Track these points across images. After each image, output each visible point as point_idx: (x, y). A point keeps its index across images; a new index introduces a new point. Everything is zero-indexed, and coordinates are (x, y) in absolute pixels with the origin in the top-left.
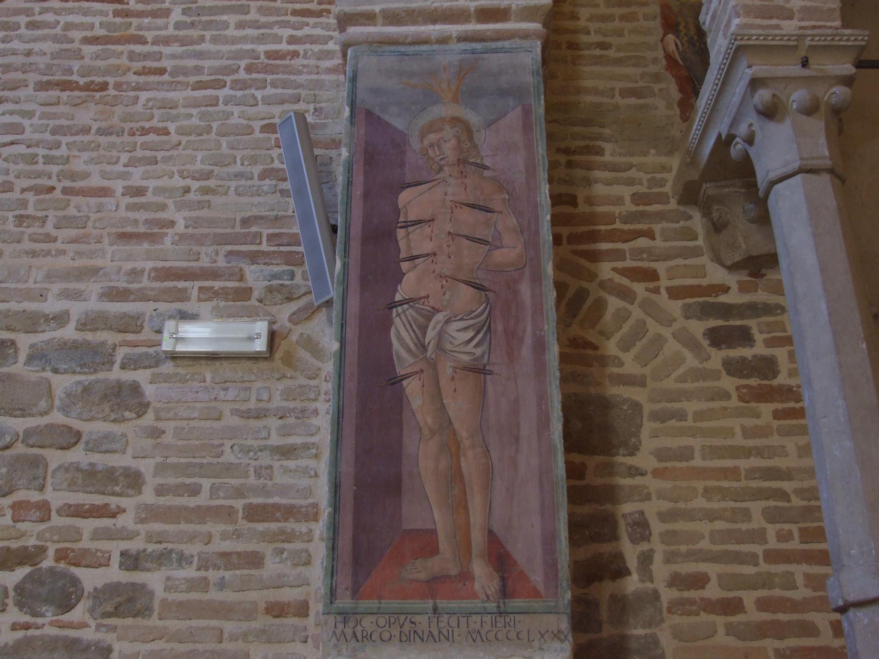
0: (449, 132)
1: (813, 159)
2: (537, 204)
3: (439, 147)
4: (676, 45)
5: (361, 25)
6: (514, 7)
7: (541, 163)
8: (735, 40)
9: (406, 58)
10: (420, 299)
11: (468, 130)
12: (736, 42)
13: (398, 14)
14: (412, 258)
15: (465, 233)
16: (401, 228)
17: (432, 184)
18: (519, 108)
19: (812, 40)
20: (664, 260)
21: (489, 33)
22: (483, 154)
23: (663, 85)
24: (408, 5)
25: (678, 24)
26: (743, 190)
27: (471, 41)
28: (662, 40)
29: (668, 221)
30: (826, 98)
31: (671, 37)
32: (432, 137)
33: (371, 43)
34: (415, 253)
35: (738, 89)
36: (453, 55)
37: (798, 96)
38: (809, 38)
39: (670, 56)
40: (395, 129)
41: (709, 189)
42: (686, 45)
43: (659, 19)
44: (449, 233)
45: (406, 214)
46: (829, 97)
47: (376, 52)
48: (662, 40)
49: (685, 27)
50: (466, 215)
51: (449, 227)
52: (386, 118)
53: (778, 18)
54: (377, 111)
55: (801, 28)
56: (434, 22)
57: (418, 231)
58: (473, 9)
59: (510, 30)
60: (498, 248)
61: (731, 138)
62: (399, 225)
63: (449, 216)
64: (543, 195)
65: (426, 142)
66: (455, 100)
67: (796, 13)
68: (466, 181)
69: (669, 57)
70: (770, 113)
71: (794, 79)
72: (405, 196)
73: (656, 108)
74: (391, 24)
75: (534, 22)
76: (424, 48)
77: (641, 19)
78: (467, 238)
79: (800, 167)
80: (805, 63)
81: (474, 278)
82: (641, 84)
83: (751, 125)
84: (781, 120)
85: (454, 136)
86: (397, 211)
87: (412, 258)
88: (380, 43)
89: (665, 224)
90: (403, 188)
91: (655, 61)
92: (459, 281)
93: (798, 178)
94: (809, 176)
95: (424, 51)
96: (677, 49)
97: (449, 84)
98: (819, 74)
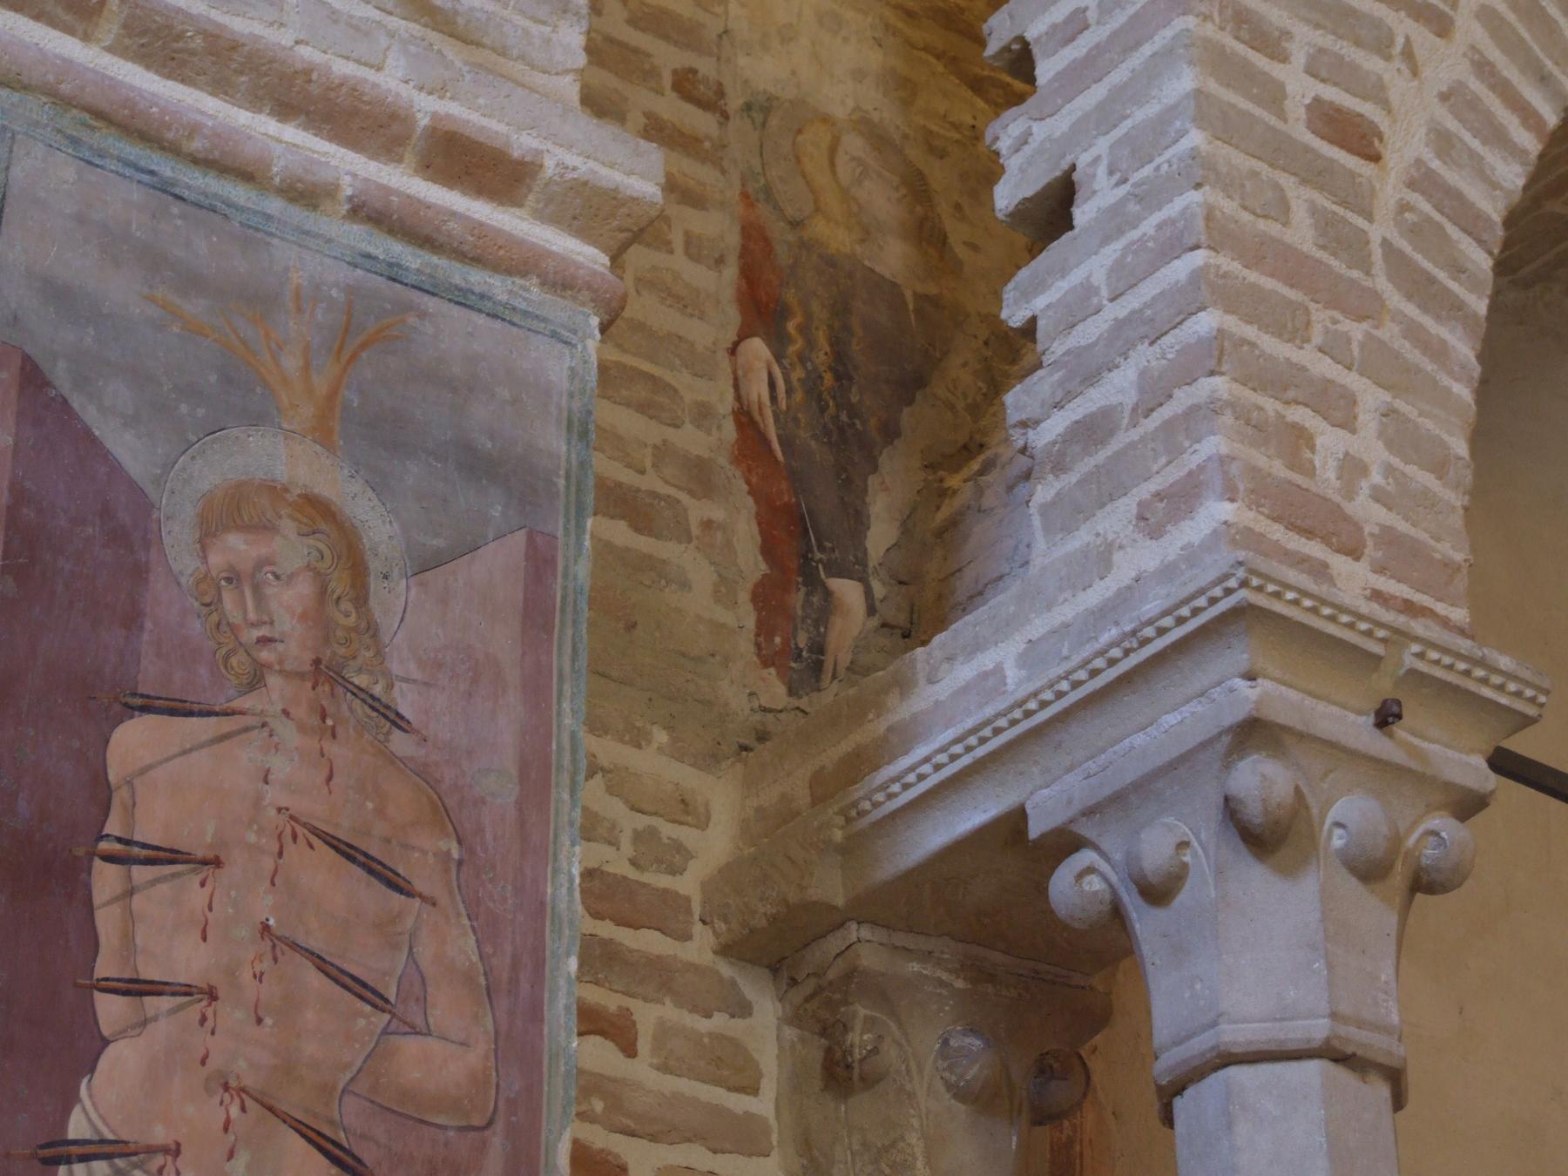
0: (291, 548)
1: (1361, 1024)
2: (543, 904)
3: (257, 590)
4: (772, 385)
5: (37, 17)
6: (549, 164)
7: (566, 761)
8: (1244, 584)
9: (176, 208)
10: (151, 1150)
11: (351, 557)
12: (1244, 593)
13: (180, 37)
14: (137, 988)
15: (315, 944)
16: (109, 858)
17: (227, 724)
18: (520, 537)
19: (1420, 656)
20: (654, 1138)
22: (395, 668)
23: (718, 514)
24: (215, 15)
25: (784, 313)
26: (960, 984)
27: (391, 232)
28: (733, 351)
29: (679, 1004)
30: (1411, 842)
31: (757, 347)
32: (237, 547)
33: (64, 102)
34: (149, 972)
35: (1171, 719)
36: (321, 258)
37: (1349, 814)
38: (1416, 648)
39: (748, 414)
40: (116, 469)
41: (868, 948)
42: (799, 396)
43: (731, 272)
44: (266, 928)
45: (130, 810)
46: (1418, 841)
47: (75, 142)
48: (733, 351)
50: (317, 871)
51: (264, 906)
52: (90, 414)
53: (1326, 540)
54: (60, 375)
55: (1377, 596)
56: (285, 110)
57: (164, 888)
58: (424, 121)
59: (521, 243)
60: (416, 1032)
61: (1065, 843)
62: (104, 846)
63: (268, 863)
64: (563, 878)
65: (216, 559)
66: (322, 433)
67: (1370, 543)
68: (333, 749)
69: (745, 418)
70: (1265, 838)
71: (1353, 754)
72: (133, 742)
73: (685, 585)
74: (144, 57)
75: (594, 242)
76: (238, 193)
78: (321, 964)
79: (1328, 1040)
80: (1386, 718)
81: (332, 1122)
82: (650, 482)
83: (1183, 845)
84: (1289, 871)
85: (308, 567)
86: (101, 794)
87: (137, 988)
88: (98, 114)
89: (669, 1011)
90: (131, 710)
91: (703, 414)
92: (285, 1119)
93: (1313, 1067)
94: (1341, 1074)
95: (241, 209)
97: (307, 367)
98: (1413, 765)
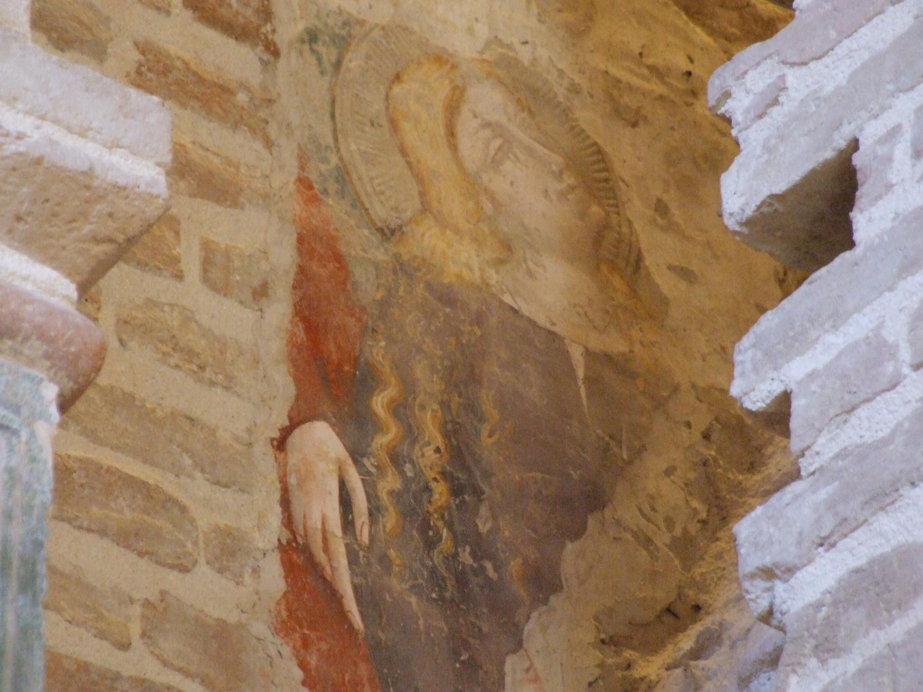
21: (29, 287)
28: (281, 444)
31: (322, 440)
39: (306, 550)
42: (390, 520)
43: (280, 310)
48: (281, 444)
49: (399, 409)
69: (298, 557)
75: (50, 258)
77: (192, 264)
91: (228, 550)
96: (348, 524)
